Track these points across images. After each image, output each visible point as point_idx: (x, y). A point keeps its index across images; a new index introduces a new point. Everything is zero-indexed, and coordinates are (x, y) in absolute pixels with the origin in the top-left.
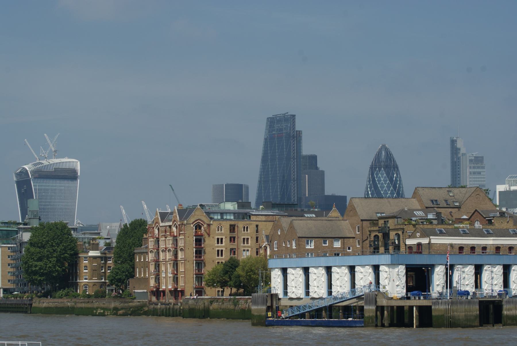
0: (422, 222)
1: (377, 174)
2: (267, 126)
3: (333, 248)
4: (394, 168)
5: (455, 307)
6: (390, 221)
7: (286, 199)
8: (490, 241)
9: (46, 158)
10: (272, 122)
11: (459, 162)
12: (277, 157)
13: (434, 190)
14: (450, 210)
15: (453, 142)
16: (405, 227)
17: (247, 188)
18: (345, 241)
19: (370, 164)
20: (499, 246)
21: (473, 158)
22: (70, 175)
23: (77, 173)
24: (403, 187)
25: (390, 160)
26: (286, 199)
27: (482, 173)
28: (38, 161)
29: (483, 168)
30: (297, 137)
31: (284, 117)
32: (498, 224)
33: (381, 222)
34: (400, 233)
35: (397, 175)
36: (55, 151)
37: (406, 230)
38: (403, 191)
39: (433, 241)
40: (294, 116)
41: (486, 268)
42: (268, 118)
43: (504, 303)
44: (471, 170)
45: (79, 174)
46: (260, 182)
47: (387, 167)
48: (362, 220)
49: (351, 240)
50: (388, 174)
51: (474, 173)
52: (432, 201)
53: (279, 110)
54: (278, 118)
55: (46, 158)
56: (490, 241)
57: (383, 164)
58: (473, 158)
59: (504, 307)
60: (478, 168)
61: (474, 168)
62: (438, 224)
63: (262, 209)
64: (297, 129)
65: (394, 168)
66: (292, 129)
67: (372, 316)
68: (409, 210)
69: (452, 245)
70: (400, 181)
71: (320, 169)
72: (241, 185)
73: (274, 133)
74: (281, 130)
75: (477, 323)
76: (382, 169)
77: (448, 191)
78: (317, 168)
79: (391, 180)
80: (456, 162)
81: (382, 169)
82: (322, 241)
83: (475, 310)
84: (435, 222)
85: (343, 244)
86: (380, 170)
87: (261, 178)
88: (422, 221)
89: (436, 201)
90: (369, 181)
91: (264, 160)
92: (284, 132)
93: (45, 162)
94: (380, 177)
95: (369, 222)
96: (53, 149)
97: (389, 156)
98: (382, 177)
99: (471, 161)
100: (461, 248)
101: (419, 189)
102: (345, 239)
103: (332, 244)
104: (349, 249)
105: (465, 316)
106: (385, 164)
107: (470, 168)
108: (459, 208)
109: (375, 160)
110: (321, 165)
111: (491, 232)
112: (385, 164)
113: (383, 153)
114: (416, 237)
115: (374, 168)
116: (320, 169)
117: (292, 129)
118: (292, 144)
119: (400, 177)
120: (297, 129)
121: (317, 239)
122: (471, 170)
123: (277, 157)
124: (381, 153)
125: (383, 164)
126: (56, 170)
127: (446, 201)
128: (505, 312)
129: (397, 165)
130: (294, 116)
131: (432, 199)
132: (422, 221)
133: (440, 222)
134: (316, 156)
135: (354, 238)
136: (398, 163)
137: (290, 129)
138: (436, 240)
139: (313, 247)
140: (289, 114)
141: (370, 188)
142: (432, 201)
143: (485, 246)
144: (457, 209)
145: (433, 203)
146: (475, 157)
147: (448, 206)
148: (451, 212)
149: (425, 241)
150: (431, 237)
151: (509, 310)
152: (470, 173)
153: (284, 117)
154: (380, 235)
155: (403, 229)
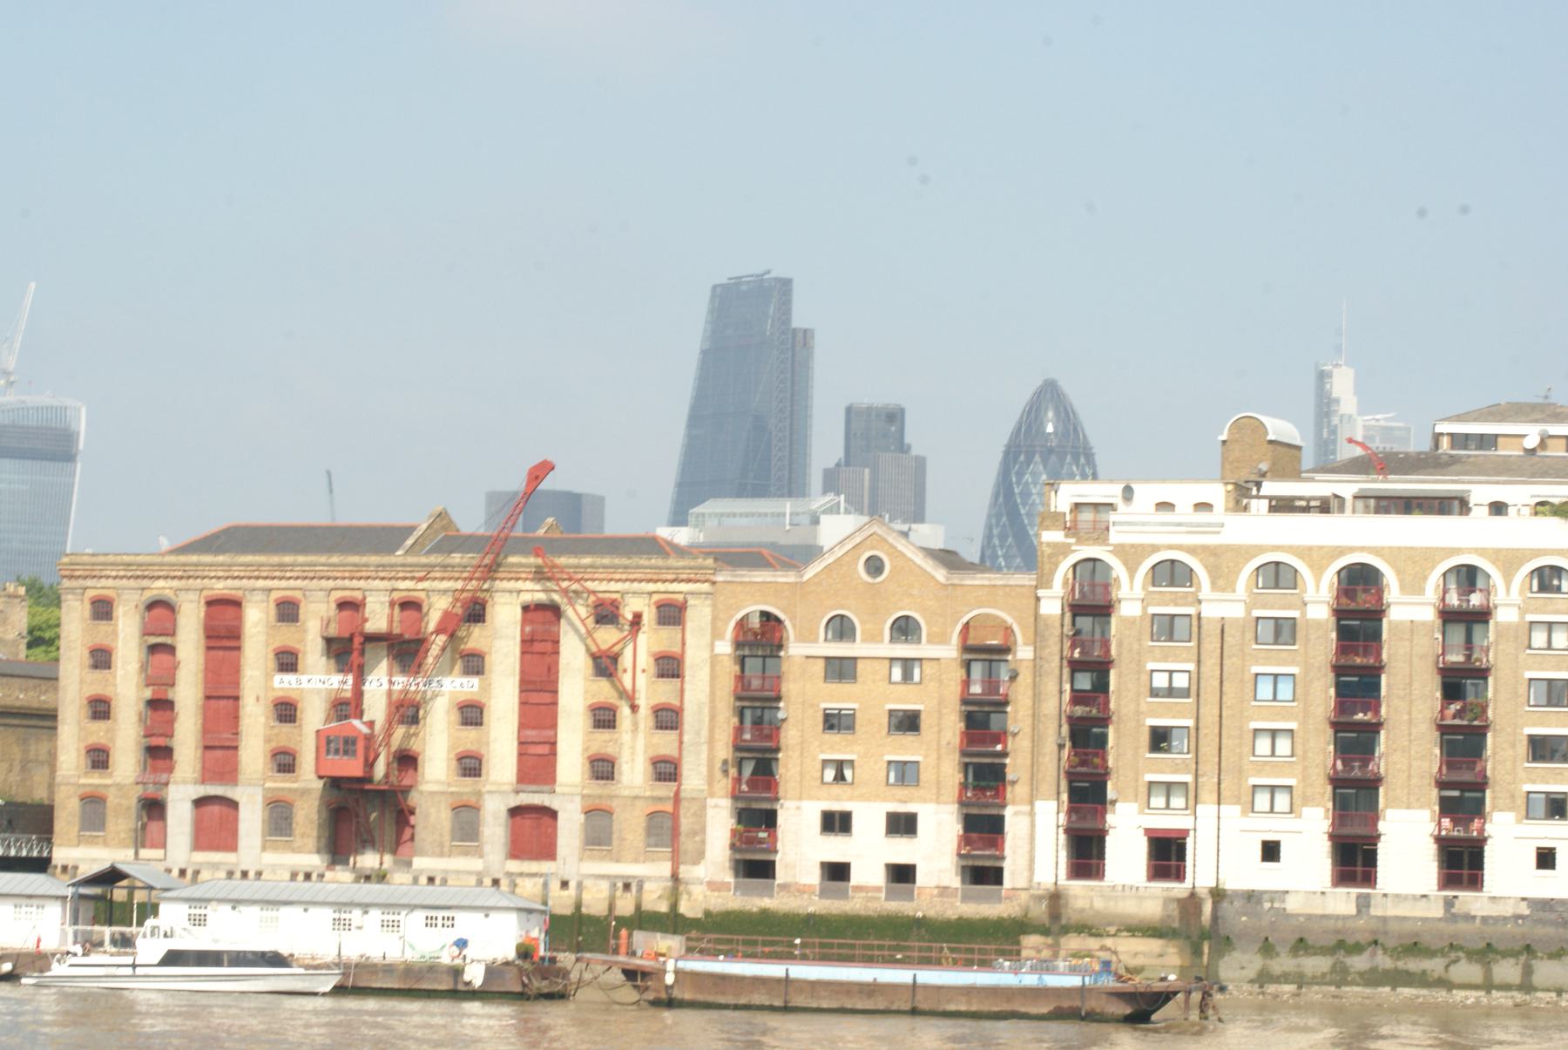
1: (1020, 475)
53: (746, 264)
54: (744, 288)
76: (1037, 458)
78: (903, 448)
86: (1029, 461)
91: (695, 419)
110: (913, 435)
116: (915, 452)
140: (772, 275)
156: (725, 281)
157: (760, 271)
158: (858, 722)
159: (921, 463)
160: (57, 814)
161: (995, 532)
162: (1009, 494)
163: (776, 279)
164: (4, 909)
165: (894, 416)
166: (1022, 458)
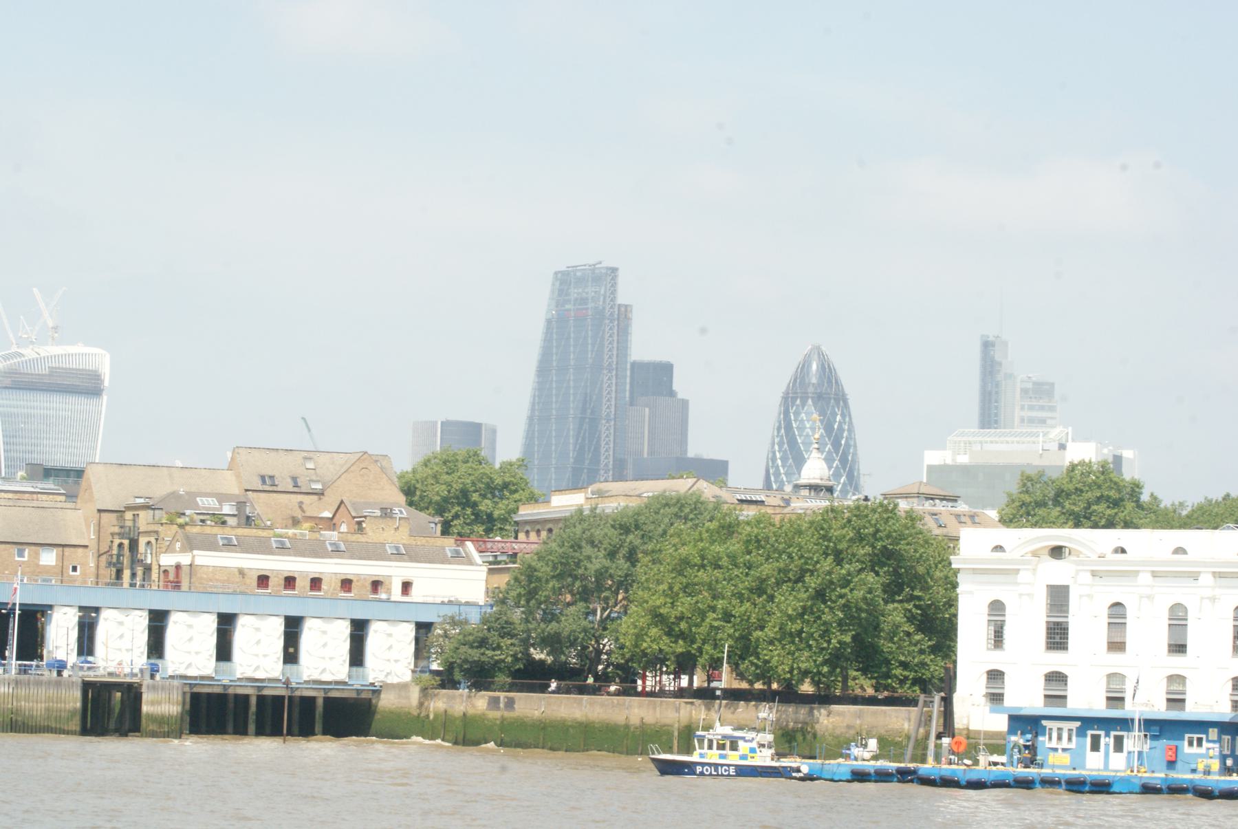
0: (203, 521)
1: (797, 414)
2: (553, 292)
3: (38, 565)
4: (837, 401)
5: (22, 692)
6: (142, 514)
7: (587, 462)
8: (331, 568)
9: (32, 343)
10: (565, 281)
11: (997, 393)
12: (572, 363)
13: (273, 454)
14: (300, 498)
15: (987, 345)
16: (160, 529)
17: (494, 432)
18: (66, 554)
19: (784, 388)
20: (349, 577)
21: (1030, 386)
22: (87, 386)
23: (102, 381)
24: (855, 446)
25: (830, 382)
26: (587, 462)
27: (1049, 422)
28: (14, 349)
29: (1052, 409)
30: (622, 317)
31: (593, 270)
32: (375, 533)
33: (129, 515)
34: (153, 540)
35: (843, 416)
36: (55, 328)
37: (162, 536)
38: (855, 454)
39: (198, 561)
40: (614, 270)
41: (104, 614)
42: (556, 273)
43: (144, 689)
44: (1023, 414)
45: (106, 383)
46: (531, 419)
47: (820, 398)
48: (100, 511)
49: (80, 550)
50: (822, 413)
51: (1031, 421)
52: (263, 478)
53: (581, 256)
54: (579, 274)
55: (32, 343)
56: (331, 568)
57: (811, 389)
58: (1030, 386)
59: (144, 697)
60: (1042, 408)
61: (1031, 408)
62: (239, 526)
63: (23, 478)
64: (621, 300)
65: (837, 401)
66: (608, 300)
67: (170, 717)
68: (187, 493)
69: (241, 572)
70: (850, 430)
71: (680, 396)
72: (479, 426)
73: (567, 307)
74: (584, 301)
75: (75, 724)
76: (810, 401)
77: (305, 458)
78: (672, 394)
79: (828, 428)
80: (990, 393)
81: (810, 401)
82: (15, 549)
83: (74, 700)
84: (232, 521)
85: (62, 558)
86: (804, 404)
87: (533, 410)
88: (202, 517)
89: (272, 477)
90: (779, 429)
91: (543, 370)
92: (591, 305)
93: (29, 353)
94: (802, 421)
95: (115, 515)
96: (51, 324)
97: (828, 373)
98: (810, 421)
99: (1025, 391)
100: (263, 580)
101: (240, 450)
102: (66, 549)
103: (37, 555)
104: (75, 569)
105: (48, 709)
106: (818, 392)
107: (1022, 408)
108: (320, 494)
109: (795, 380)
110: (680, 385)
111: (343, 547)
112: (818, 392)
113: (814, 367)
114: (174, 551)
115: (794, 396)
116: (680, 396)
117: (608, 300)
118: (607, 336)
119: (851, 423)
120: (621, 300)
121: (33, 548)
122: (1023, 414)
123: (572, 363)
124: (810, 366)
125: (811, 389)
126: (53, 371)
127: (294, 479)
128: (145, 708)
129: (844, 395)
130: (614, 270)
131: (263, 473)
132: (202, 517)
133: (243, 521)
134: (671, 366)
135: (86, 547)
136: (848, 389)
137: (604, 302)
138: (204, 558)
139: (26, 559)
140: (604, 265)
141: (781, 444)
142: (263, 478)
143: (317, 576)
144: (315, 497)
145: (264, 482)
146: (1035, 383)
147: (296, 490)
148: (301, 503)
149: (185, 559)
150: (195, 552)
151: (153, 703)
152: (1022, 420)
153: (593, 270)
154: (126, 542)
155: (157, 532)
156: (564, 268)
157: (592, 262)
158: (308, 584)
159: (685, 404)
160: (347, 658)
161: (778, 455)
162: (789, 428)
163: (608, 268)
164: (1236, 787)
165: (665, 370)
166: (798, 402)
